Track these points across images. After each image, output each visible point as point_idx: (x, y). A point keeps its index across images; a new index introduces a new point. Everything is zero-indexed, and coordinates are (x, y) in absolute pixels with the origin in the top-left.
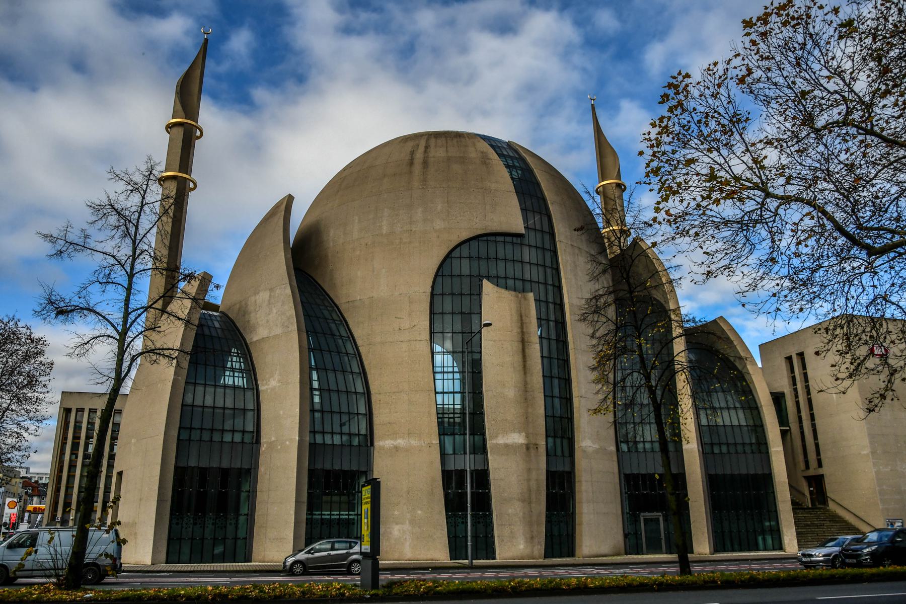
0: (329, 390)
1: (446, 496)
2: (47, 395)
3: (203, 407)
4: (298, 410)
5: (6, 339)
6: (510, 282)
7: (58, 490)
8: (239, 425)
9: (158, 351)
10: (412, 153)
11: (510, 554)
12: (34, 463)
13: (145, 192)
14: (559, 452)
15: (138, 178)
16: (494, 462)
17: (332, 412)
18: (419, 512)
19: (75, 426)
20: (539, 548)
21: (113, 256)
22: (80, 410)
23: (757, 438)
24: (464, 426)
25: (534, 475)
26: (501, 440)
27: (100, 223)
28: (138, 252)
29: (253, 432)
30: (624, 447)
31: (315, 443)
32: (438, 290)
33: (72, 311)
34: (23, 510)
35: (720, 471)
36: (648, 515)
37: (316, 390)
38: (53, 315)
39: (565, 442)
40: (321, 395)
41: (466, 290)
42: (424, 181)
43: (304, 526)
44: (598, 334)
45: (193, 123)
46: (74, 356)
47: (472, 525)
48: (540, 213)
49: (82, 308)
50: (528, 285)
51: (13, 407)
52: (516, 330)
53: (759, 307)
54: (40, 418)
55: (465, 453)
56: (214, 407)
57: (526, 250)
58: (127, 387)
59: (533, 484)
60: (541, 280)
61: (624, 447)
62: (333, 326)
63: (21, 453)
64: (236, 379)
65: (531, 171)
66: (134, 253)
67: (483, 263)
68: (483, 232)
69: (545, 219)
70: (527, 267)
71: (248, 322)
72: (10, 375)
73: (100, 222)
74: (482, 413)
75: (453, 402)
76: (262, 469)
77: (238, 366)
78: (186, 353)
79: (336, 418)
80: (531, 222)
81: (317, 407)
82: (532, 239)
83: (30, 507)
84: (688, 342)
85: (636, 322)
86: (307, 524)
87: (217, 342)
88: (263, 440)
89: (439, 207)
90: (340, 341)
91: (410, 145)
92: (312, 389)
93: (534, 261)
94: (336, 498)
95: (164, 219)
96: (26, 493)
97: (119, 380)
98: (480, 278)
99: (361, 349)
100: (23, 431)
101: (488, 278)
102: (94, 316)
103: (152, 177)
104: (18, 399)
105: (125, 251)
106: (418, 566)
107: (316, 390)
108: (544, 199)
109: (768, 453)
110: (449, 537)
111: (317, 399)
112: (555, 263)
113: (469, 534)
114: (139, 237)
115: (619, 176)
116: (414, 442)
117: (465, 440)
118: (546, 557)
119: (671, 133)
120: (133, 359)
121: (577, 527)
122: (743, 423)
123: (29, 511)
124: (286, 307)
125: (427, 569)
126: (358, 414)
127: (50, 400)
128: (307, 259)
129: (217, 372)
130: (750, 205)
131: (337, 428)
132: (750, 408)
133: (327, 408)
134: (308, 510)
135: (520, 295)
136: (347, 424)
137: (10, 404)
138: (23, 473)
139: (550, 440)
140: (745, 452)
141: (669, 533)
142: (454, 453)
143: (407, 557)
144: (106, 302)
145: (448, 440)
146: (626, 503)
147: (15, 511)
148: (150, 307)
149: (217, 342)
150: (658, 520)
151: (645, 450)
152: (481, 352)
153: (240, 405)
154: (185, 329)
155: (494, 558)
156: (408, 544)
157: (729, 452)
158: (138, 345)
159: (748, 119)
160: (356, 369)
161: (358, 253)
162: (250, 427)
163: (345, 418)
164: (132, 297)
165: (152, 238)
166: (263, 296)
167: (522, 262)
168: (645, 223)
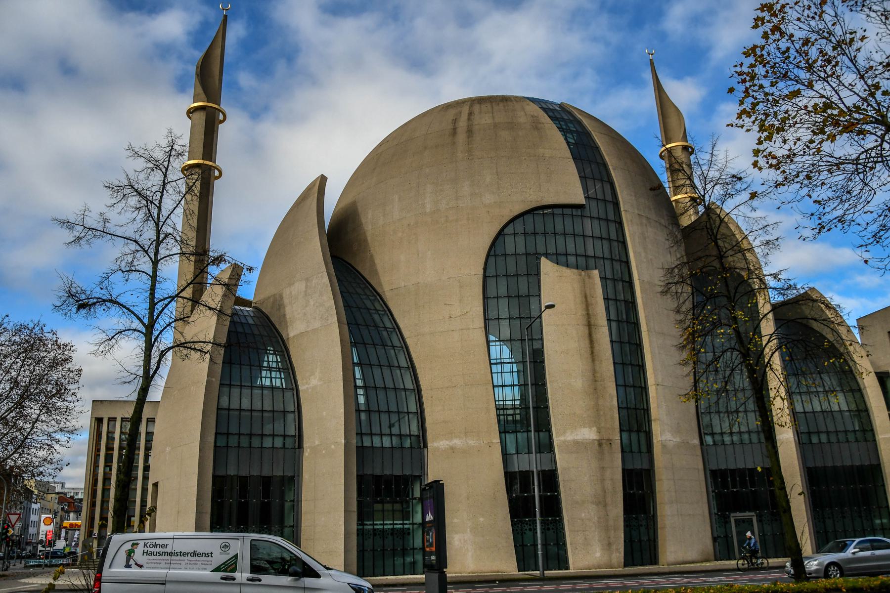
0: (376, 388)
1: (511, 501)
2: (76, 404)
3: (240, 410)
4: (342, 411)
5: (32, 345)
6: (572, 259)
7: (93, 505)
8: (279, 430)
9: (188, 345)
10: (455, 121)
11: (581, 565)
12: (70, 478)
13: (167, 169)
14: (635, 448)
15: (159, 155)
16: (562, 460)
17: (379, 412)
18: (482, 519)
19: (108, 436)
20: (618, 555)
21: (136, 241)
22: (112, 420)
23: (861, 423)
24: (527, 420)
25: (608, 473)
26: (570, 437)
27: (120, 206)
28: (162, 236)
29: (295, 436)
30: (709, 440)
31: (363, 447)
32: (491, 271)
33: (94, 304)
34: (60, 527)
35: (819, 464)
36: (739, 515)
37: (360, 387)
38: (74, 309)
39: (642, 435)
40: (367, 396)
41: (523, 270)
42: (470, 151)
43: (354, 537)
44: (684, 309)
45: (210, 163)
46: (101, 359)
47: (542, 533)
48: (602, 180)
49: (104, 301)
50: (592, 262)
51: (43, 417)
52: (581, 312)
53: (885, 263)
54: (70, 429)
55: (530, 452)
56: (251, 410)
57: (587, 222)
58: (156, 394)
59: (608, 485)
60: (607, 255)
61: (709, 440)
62: (376, 317)
63: (53, 466)
64: (274, 380)
65: (588, 135)
66: (158, 237)
67: (540, 240)
68: (539, 204)
69: (607, 187)
70: (590, 242)
71: (285, 315)
72: (38, 384)
73: (119, 204)
74: (547, 407)
75: (511, 396)
76: (306, 476)
77: (274, 365)
78: (219, 345)
79: (384, 417)
80: (591, 192)
81: (362, 408)
82: (594, 209)
83: (66, 523)
84: (776, 320)
85: (728, 291)
86: (358, 535)
87: (251, 340)
88: (306, 445)
89: (488, 180)
90: (385, 333)
91: (452, 113)
92: (356, 387)
93: (597, 233)
94: (388, 507)
95: (188, 197)
96: (63, 509)
97: (148, 378)
98: (537, 256)
99: (408, 341)
100: (54, 442)
101: (546, 255)
102: (118, 309)
103: (173, 153)
104: (47, 409)
105: (150, 234)
106: (483, 579)
107: (360, 387)
108: (605, 165)
109: (875, 440)
110: (515, 546)
111: (362, 400)
112: (620, 235)
113: (539, 541)
114: (162, 219)
115: (685, 138)
116: (472, 442)
117: (529, 440)
118: (625, 565)
119: (768, 63)
120: (162, 354)
121: (659, 531)
122: (844, 407)
123: (65, 528)
124: (325, 298)
125: (494, 581)
126: (408, 413)
127: (80, 409)
128: (344, 244)
129: (253, 374)
130: (870, 142)
131: (386, 430)
132: (852, 391)
133: (374, 407)
134: (358, 520)
135: (583, 273)
136: (397, 425)
137: (39, 415)
138: (58, 489)
139: (625, 435)
140: (848, 441)
141: (764, 535)
142: (517, 453)
143: (470, 570)
144: (131, 293)
145: (510, 438)
146: (714, 503)
147: (51, 528)
148: (177, 296)
149: (251, 340)
150: (751, 520)
151: (733, 443)
152: (542, 339)
153: (279, 407)
154: (218, 320)
155: (567, 568)
156: (470, 554)
157: (829, 442)
158: (167, 339)
159: (863, 38)
160: (403, 363)
161: (400, 234)
162: (291, 431)
163: (394, 417)
164: (157, 285)
165: (178, 219)
166: (299, 287)
167: (584, 236)
168: (734, 176)
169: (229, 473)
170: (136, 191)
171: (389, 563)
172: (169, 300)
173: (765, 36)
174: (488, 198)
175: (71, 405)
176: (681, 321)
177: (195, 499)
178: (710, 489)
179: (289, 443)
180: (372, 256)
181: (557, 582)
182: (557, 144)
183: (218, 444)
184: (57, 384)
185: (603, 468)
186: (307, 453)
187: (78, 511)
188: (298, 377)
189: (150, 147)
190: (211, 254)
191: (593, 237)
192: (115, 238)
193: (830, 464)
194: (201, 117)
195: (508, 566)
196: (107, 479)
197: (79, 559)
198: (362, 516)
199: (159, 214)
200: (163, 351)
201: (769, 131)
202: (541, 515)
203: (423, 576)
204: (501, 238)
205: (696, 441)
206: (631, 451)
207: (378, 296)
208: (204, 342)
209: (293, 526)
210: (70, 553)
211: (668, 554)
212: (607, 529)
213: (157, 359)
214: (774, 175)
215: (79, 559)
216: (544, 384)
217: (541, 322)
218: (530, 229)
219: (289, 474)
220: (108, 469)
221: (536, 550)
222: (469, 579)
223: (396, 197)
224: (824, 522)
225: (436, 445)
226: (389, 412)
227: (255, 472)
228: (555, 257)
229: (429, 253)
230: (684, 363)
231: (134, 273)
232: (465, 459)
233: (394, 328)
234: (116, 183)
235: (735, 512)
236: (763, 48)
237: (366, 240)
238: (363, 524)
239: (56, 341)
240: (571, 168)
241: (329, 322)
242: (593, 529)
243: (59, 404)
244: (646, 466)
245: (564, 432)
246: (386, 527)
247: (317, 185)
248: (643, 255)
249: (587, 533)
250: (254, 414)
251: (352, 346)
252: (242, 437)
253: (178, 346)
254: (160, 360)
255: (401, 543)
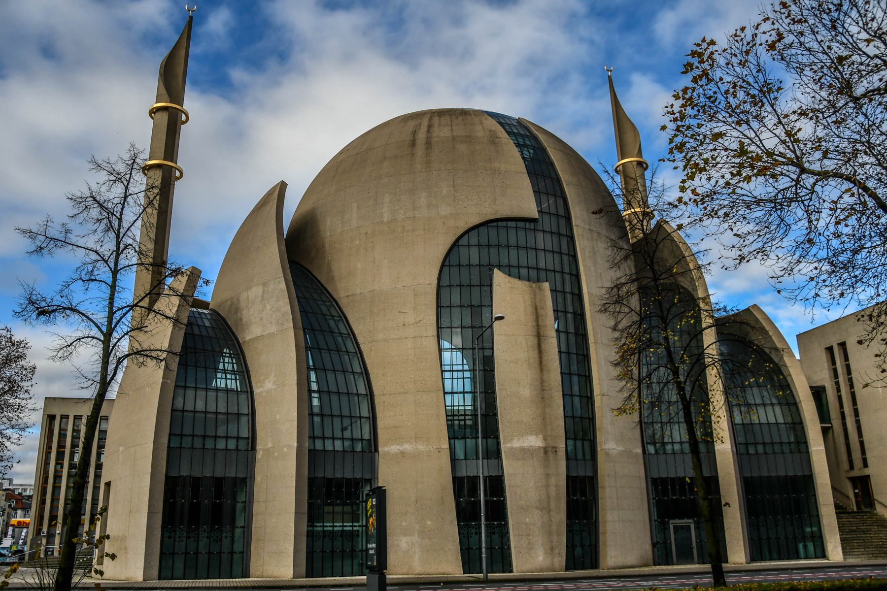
2: (29, 401)
3: (194, 412)
4: (295, 414)
6: (524, 271)
7: (43, 502)
8: (233, 432)
9: (145, 353)
10: (414, 133)
11: (524, 568)
12: (17, 474)
13: (128, 182)
14: (580, 456)
15: (121, 168)
18: (429, 523)
19: (60, 434)
20: (560, 560)
21: (96, 252)
23: (796, 436)
24: (476, 429)
25: (553, 481)
26: (517, 444)
28: (122, 246)
29: (248, 438)
30: (651, 449)
33: (54, 311)
35: (756, 474)
37: (314, 392)
38: (34, 316)
39: (587, 444)
40: (320, 398)
41: (475, 281)
42: (428, 163)
43: (304, 539)
44: (620, 327)
46: (59, 358)
47: (486, 536)
48: (555, 196)
49: (64, 308)
50: (543, 274)
52: (531, 323)
54: (22, 426)
55: (477, 458)
56: (206, 412)
57: (540, 236)
58: (113, 393)
59: (553, 491)
60: (558, 268)
61: (651, 449)
62: (332, 323)
64: (229, 381)
65: (543, 150)
66: (118, 248)
68: (493, 217)
69: (560, 202)
70: (541, 255)
71: (241, 319)
73: (81, 215)
74: (496, 415)
75: (462, 403)
76: (258, 478)
79: (337, 421)
81: (316, 410)
82: (547, 223)
83: (14, 521)
84: (719, 333)
85: (662, 312)
86: (308, 536)
87: (207, 342)
88: (259, 446)
89: (445, 192)
90: (340, 339)
91: (412, 124)
94: (338, 509)
95: (149, 210)
96: (10, 506)
97: (105, 384)
98: (491, 267)
99: (362, 347)
100: (5, 440)
101: (499, 267)
102: (77, 317)
103: (135, 166)
106: (428, 580)
107: (314, 392)
108: (559, 180)
109: (808, 452)
111: (316, 402)
112: (572, 248)
113: (484, 545)
114: (122, 231)
115: (640, 154)
116: (421, 447)
117: (477, 444)
118: (567, 569)
120: (119, 361)
121: (601, 536)
122: (781, 420)
123: (13, 525)
124: (281, 303)
125: (438, 583)
126: (360, 417)
127: (33, 407)
128: (302, 251)
130: (784, 182)
131: (338, 434)
132: (788, 404)
133: (327, 411)
134: (308, 522)
135: (534, 285)
139: (570, 442)
140: (782, 452)
141: (701, 541)
142: (466, 459)
143: (417, 572)
145: (459, 444)
148: (136, 305)
149: (207, 342)
150: (689, 527)
151: (674, 453)
152: (492, 349)
153: (233, 409)
155: (511, 571)
156: (417, 556)
157: (765, 453)
158: (124, 346)
159: (779, 89)
160: (357, 369)
161: (357, 242)
162: (245, 433)
163: (346, 422)
164: (116, 294)
166: (256, 291)
168: (670, 204)
169: (181, 474)
170: (98, 202)
171: (338, 564)
172: (127, 309)
173: (695, 80)
174: (445, 210)
175: (23, 403)
176: (617, 339)
177: (147, 499)
178: (651, 497)
179: (242, 445)
180: (329, 263)
181: (499, 584)
182: (513, 159)
183: (172, 445)
184: (10, 382)
185: (548, 475)
186: (259, 455)
187: (26, 509)
188: (253, 380)
189: (112, 161)
190: (168, 266)
191: (544, 250)
192: (77, 249)
193: (765, 474)
194: (164, 117)
195: (453, 568)
196: (58, 477)
197: (27, 558)
198: (312, 518)
199: (119, 225)
200: (120, 358)
201: (695, 169)
202: (486, 520)
203: (365, 577)
204: (456, 248)
205: (639, 450)
206: (576, 459)
207: (334, 302)
208: (160, 351)
209: (244, 527)
210: (17, 552)
211: (608, 558)
212: (550, 534)
213: (114, 366)
214: (698, 211)
215: (27, 558)
216: (494, 392)
217: (492, 332)
218: (484, 241)
219: (241, 475)
220: (59, 467)
221: (481, 553)
222: (414, 581)
223: (355, 205)
224: (758, 529)
225: (386, 449)
226: (341, 416)
227: (208, 474)
228: (507, 269)
229: (386, 261)
230: (620, 378)
231: (94, 283)
232: (413, 464)
233: (349, 334)
234: (79, 194)
235: (674, 519)
236: (694, 89)
237: (323, 247)
238: (313, 526)
239: (10, 338)
240: (526, 182)
241: (285, 327)
242: (537, 533)
243: (11, 401)
244: (589, 474)
245: (512, 440)
246: (336, 529)
247: (277, 191)
248: (593, 269)
249: (531, 537)
250: (209, 416)
251: (307, 351)
252: (195, 438)
253: (135, 353)
254: (117, 367)
255: (350, 544)
